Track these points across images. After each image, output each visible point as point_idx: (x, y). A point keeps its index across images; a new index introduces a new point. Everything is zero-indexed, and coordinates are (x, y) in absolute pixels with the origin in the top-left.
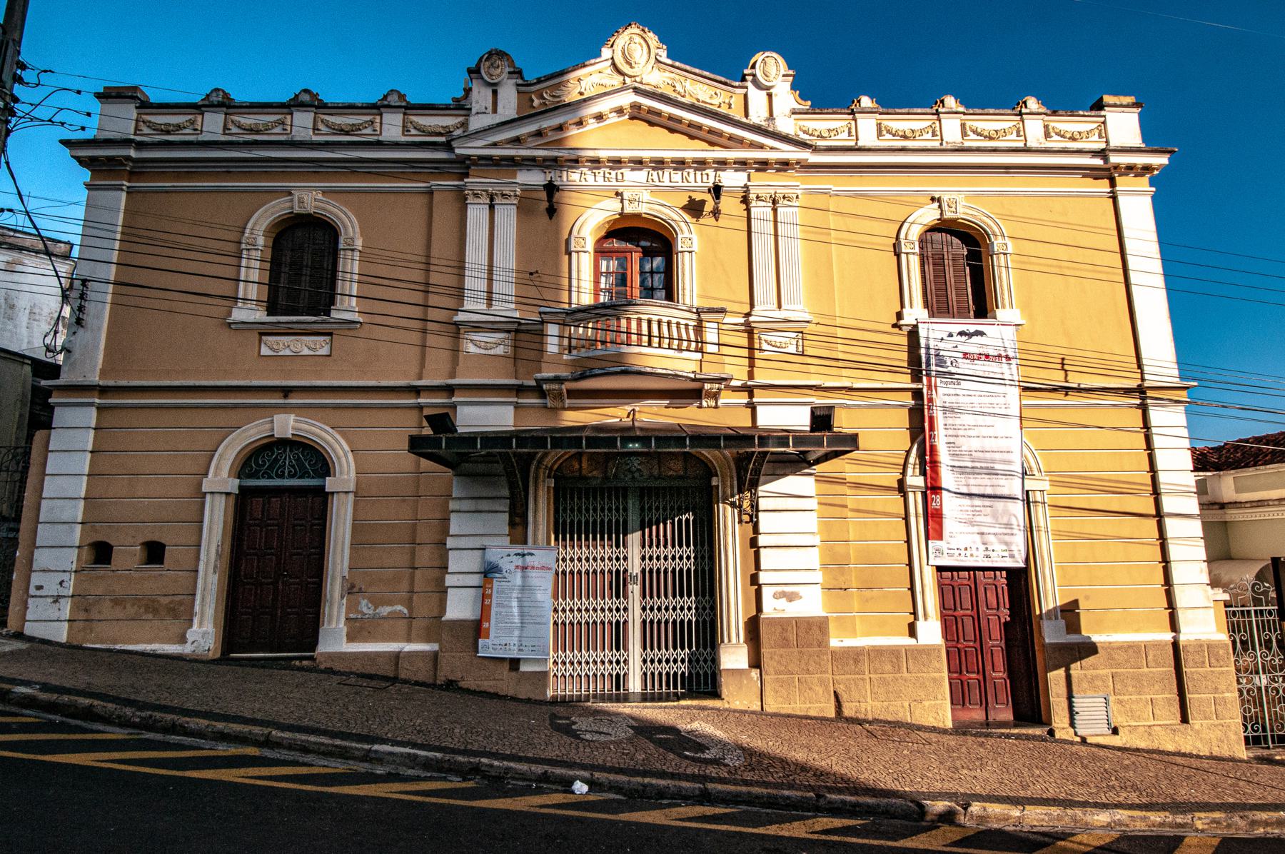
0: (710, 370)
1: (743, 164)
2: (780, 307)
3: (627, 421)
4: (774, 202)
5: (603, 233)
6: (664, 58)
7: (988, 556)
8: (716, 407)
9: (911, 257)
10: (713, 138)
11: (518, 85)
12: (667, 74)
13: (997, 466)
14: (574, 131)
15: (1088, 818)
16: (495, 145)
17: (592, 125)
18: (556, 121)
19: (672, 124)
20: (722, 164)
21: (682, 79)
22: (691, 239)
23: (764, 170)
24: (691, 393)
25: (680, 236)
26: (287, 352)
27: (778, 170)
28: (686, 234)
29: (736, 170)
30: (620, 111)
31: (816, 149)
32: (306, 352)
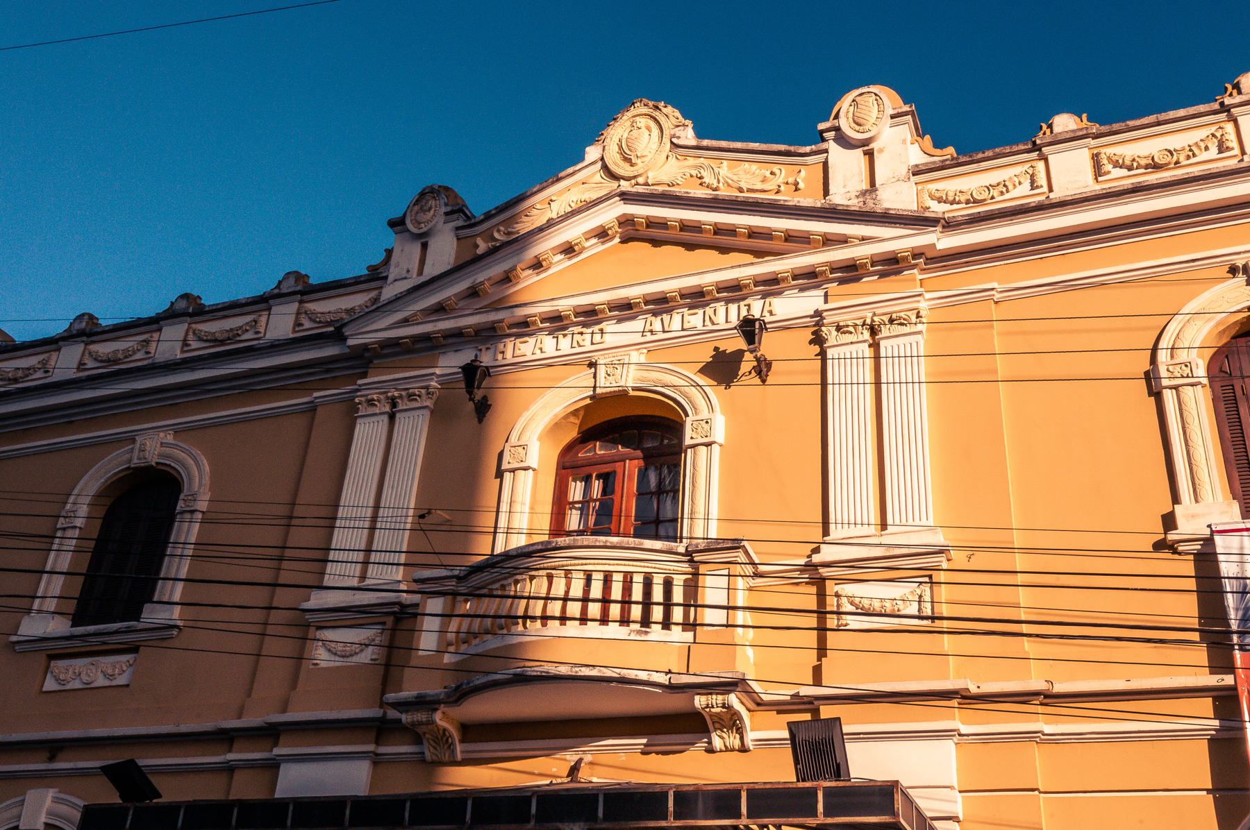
0: (708, 668)
1: (810, 278)
2: (884, 525)
3: (562, 781)
4: (873, 331)
5: (573, 434)
6: (688, 136)
8: (743, 749)
9: (1188, 392)
10: (759, 245)
11: (457, 229)
12: (691, 161)
14: (528, 280)
16: (405, 322)
17: (560, 263)
18: (496, 270)
19: (686, 236)
20: (771, 285)
21: (713, 163)
22: (711, 418)
23: (857, 279)
24: (676, 720)
25: (689, 421)
26: (77, 685)
27: (883, 275)
28: (704, 414)
29: (802, 289)
30: (602, 234)
31: (950, 225)
32: (101, 681)
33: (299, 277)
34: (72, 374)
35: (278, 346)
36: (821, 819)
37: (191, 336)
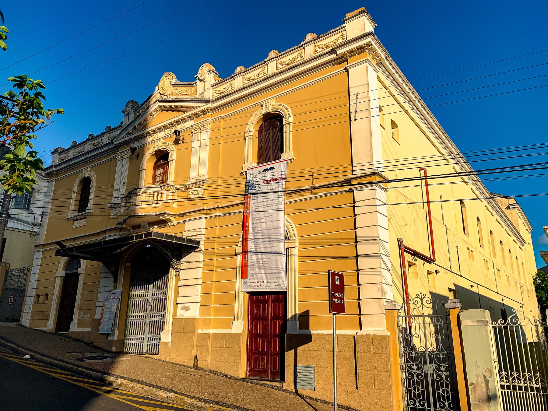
5: (156, 160)
6: (175, 81)
7: (268, 286)
13: (273, 237)
15: (158, 393)
33: (109, 127)
34: (242, 86)
35: (274, 75)
36: (144, 239)
37: (245, 81)
